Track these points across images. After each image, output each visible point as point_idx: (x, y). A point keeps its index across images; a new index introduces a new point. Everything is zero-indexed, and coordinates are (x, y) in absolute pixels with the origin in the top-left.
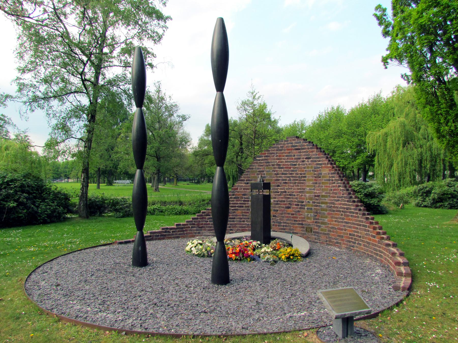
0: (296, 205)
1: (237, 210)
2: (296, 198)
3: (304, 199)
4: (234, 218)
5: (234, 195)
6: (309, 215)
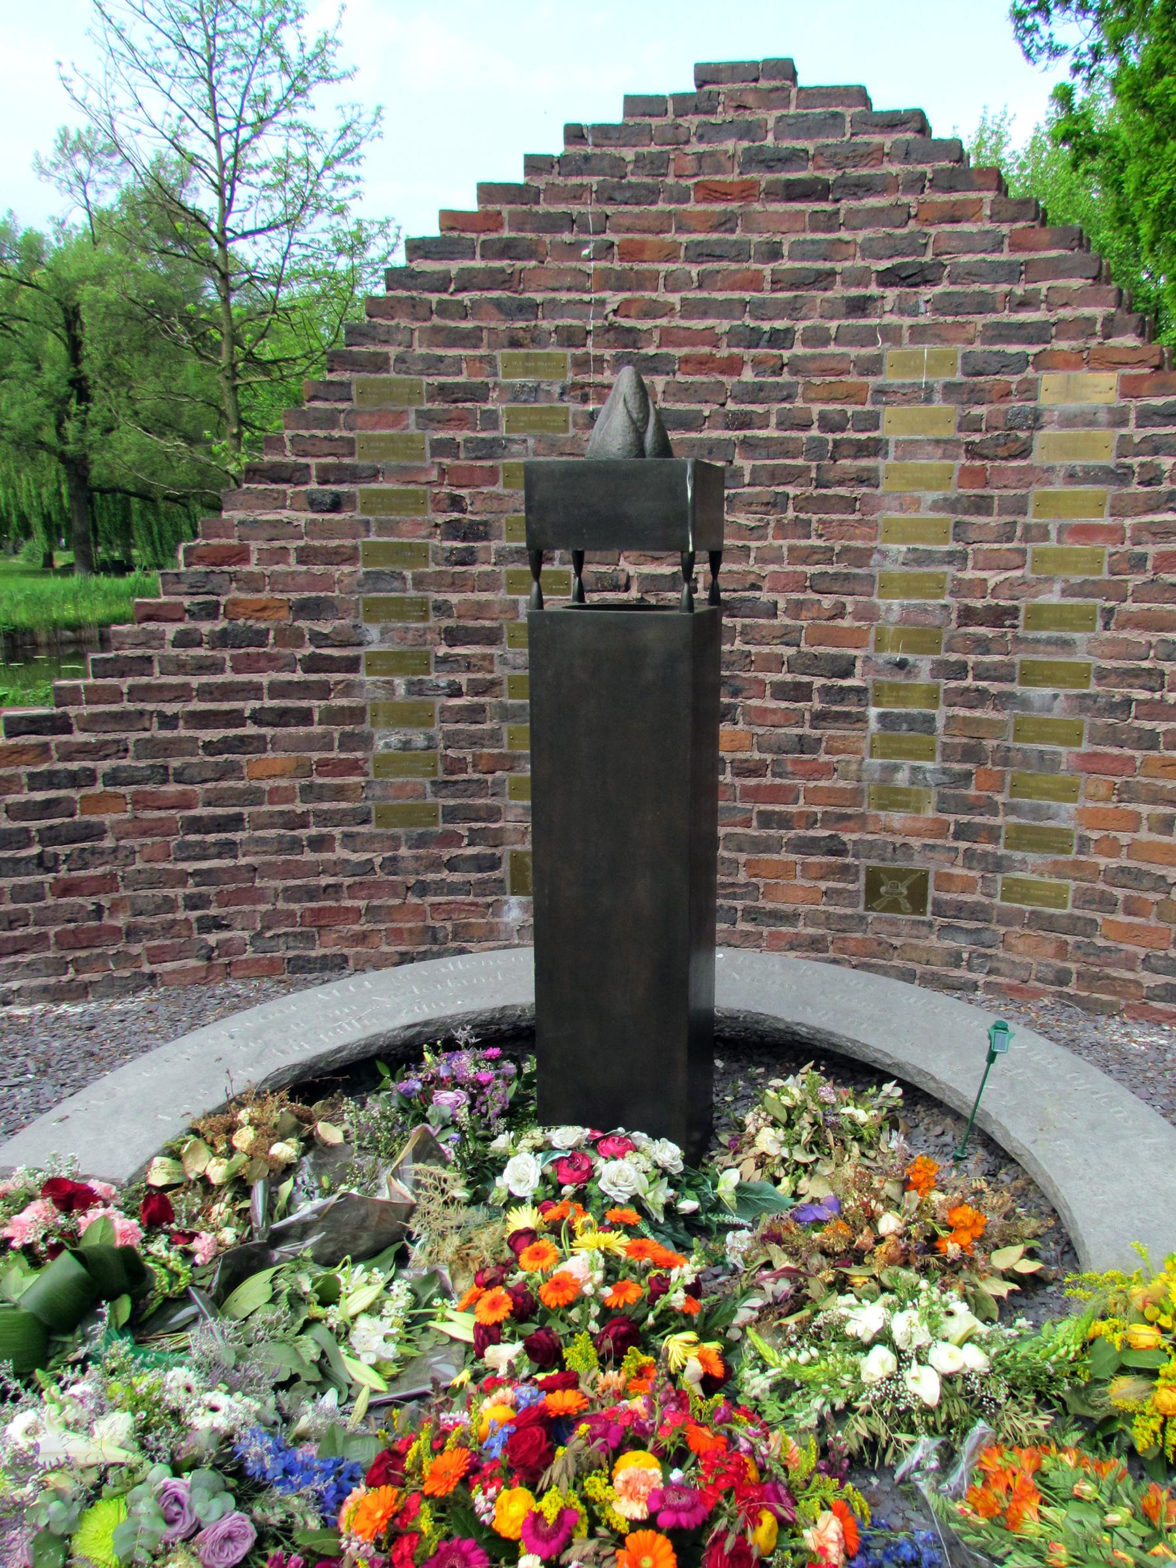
0: (782, 691)
1: (256, 745)
2: (788, 637)
3: (856, 638)
4: (235, 822)
5: (210, 611)
6: (902, 778)
